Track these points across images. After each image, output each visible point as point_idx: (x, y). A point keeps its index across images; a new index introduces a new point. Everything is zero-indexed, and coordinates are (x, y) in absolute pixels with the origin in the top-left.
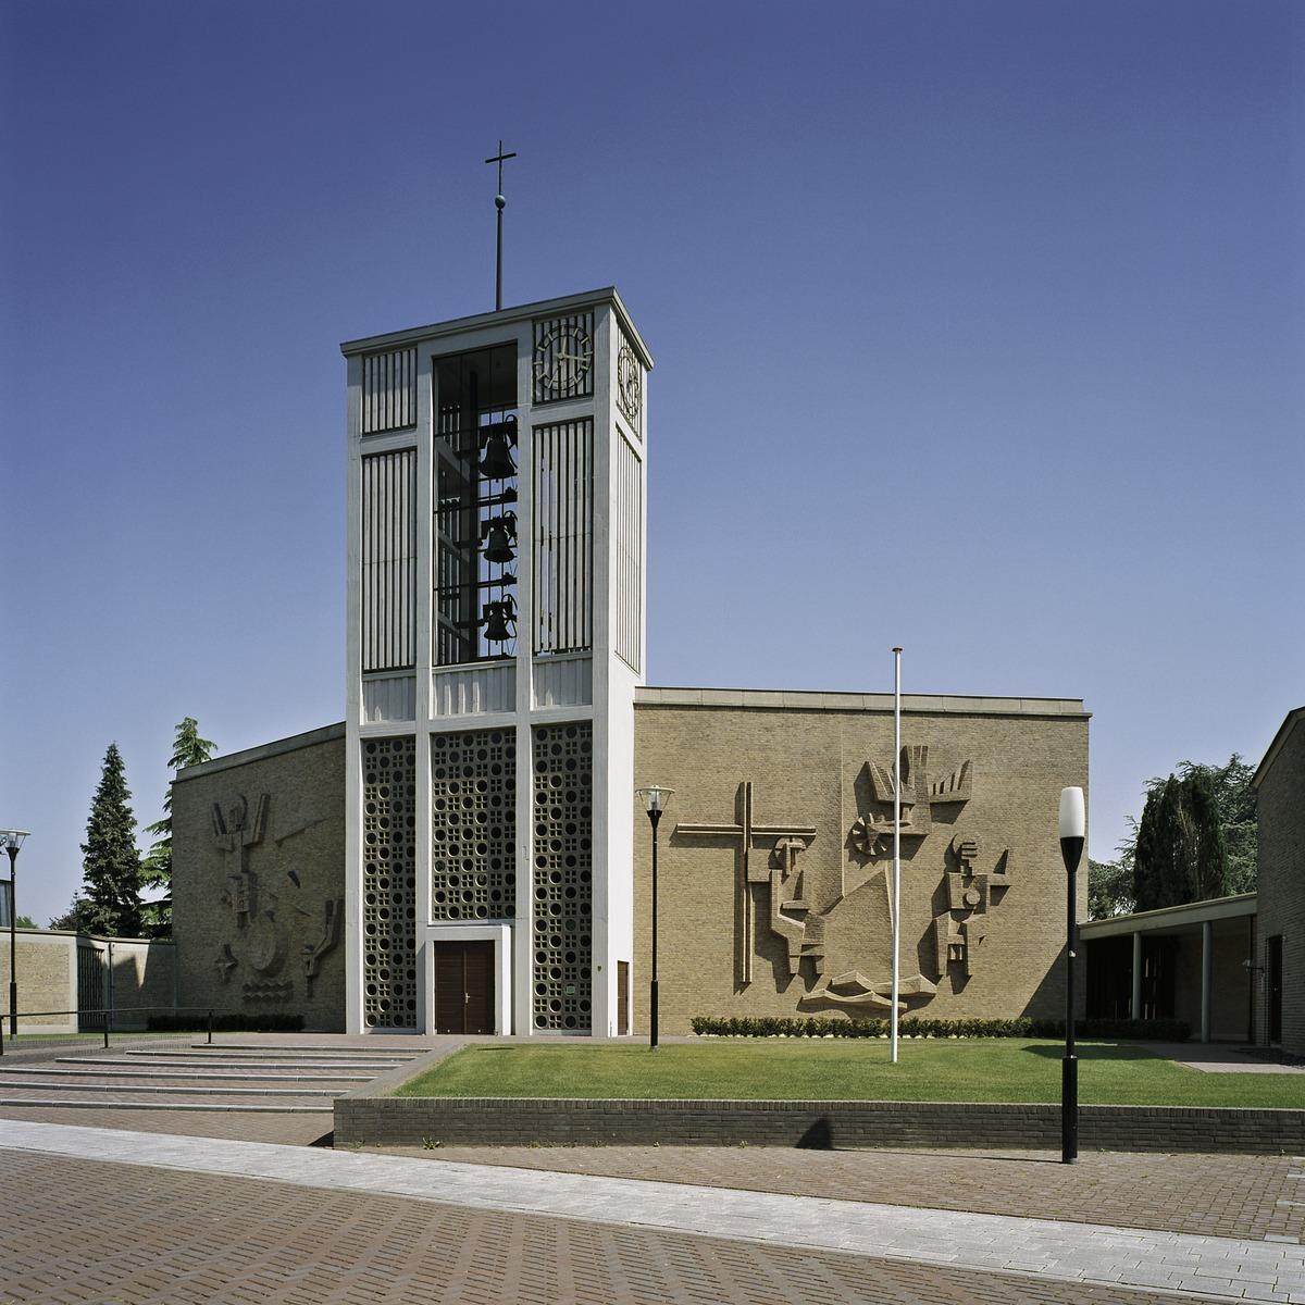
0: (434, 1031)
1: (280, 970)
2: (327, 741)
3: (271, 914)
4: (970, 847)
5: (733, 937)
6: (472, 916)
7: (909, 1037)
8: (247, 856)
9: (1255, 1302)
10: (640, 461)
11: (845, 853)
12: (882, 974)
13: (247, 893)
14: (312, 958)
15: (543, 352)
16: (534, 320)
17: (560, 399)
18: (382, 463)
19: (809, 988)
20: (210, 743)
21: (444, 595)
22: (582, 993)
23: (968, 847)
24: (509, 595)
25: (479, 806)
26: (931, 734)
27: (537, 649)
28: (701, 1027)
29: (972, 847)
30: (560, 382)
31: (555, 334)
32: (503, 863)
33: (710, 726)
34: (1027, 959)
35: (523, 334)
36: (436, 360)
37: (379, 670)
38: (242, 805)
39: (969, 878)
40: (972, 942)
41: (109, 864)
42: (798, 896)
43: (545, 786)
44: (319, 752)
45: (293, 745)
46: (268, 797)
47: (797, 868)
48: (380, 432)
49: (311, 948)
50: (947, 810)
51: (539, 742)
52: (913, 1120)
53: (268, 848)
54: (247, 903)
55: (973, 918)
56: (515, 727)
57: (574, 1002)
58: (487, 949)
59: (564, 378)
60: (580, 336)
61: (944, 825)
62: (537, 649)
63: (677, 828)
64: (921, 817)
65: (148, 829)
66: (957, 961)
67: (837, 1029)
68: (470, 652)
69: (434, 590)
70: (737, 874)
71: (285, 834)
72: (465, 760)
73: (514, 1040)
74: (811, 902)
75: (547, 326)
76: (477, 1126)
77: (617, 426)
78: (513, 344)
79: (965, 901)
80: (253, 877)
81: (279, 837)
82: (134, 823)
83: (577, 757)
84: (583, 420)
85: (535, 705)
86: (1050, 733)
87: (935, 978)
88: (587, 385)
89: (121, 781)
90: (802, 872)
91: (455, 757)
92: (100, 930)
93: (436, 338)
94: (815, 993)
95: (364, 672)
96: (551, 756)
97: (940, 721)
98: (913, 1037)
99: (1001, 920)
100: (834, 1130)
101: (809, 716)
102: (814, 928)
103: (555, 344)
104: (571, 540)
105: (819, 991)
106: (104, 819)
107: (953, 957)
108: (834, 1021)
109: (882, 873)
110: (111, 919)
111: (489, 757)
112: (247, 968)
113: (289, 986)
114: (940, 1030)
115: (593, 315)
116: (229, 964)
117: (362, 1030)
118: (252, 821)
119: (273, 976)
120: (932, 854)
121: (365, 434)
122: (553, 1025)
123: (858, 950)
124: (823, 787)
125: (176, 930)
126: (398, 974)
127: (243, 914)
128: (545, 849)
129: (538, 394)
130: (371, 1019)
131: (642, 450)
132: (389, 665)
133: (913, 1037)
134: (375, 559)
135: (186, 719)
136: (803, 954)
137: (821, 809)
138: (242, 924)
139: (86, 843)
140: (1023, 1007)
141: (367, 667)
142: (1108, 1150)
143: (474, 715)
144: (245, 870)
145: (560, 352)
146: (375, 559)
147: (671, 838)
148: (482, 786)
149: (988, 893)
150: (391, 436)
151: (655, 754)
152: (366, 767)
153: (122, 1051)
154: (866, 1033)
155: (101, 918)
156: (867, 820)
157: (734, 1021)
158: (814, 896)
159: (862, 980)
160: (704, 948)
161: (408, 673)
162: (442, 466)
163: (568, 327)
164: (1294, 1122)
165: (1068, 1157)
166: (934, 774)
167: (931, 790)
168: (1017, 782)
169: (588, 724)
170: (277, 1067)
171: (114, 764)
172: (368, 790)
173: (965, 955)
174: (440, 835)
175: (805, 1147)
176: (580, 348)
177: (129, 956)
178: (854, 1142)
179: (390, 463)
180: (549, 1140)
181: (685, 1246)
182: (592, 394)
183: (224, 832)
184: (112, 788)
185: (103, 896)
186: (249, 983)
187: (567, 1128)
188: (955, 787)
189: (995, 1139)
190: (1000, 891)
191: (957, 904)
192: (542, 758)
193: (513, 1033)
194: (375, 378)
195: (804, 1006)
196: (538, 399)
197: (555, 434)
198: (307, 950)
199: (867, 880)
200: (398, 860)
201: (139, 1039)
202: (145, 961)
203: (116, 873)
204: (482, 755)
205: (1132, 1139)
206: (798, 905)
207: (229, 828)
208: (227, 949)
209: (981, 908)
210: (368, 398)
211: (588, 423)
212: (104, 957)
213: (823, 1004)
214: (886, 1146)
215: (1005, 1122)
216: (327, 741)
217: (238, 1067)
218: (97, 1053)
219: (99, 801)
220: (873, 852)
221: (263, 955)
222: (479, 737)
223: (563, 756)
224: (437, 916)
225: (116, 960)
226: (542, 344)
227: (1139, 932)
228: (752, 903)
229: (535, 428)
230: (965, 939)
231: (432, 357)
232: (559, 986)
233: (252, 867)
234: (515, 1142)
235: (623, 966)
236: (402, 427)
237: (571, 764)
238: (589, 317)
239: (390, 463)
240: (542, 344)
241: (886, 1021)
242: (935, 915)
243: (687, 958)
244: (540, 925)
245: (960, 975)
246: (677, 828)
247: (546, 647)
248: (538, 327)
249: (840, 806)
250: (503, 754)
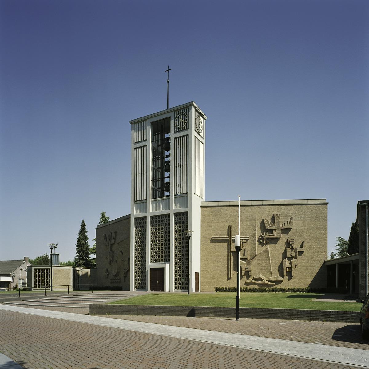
0: (150, 290)
2: (125, 219)
3: (116, 261)
4: (293, 241)
5: (227, 266)
7: (274, 292)
9: (364, 367)
10: (203, 144)
11: (257, 243)
12: (268, 275)
13: (111, 256)
14: (125, 272)
16: (174, 111)
17: (180, 131)
18: (139, 149)
19: (248, 279)
20: (108, 218)
21: (154, 181)
23: (292, 240)
25: (161, 234)
26: (281, 210)
27: (175, 194)
28: (217, 289)
29: (293, 240)
30: (181, 126)
31: (180, 114)
32: (167, 248)
33: (221, 211)
34: (309, 271)
35: (172, 115)
36: (152, 123)
37: (138, 201)
38: (111, 234)
39: (292, 249)
40: (293, 267)
41: (82, 249)
42: (244, 255)
43: (177, 228)
44: (127, 221)
45: (122, 219)
46: (116, 232)
47: (244, 247)
48: (139, 142)
49: (125, 269)
50: (286, 231)
51: (176, 217)
52: (211, 311)
54: (111, 258)
55: (294, 260)
56: (170, 214)
57: (184, 283)
58: (162, 270)
59: (182, 125)
61: (285, 235)
62: (175, 194)
63: (212, 238)
64: (278, 233)
65: (94, 240)
66: (289, 272)
67: (254, 290)
68: (162, 195)
69: (151, 180)
70: (228, 249)
72: (158, 222)
73: (169, 293)
74: (248, 256)
75: (178, 112)
76: (118, 311)
77: (195, 136)
78: (170, 117)
79: (291, 255)
81: (118, 242)
82: (88, 239)
83: (144, 225)
84: (186, 135)
85: (175, 208)
86: (316, 208)
87: (283, 276)
88: (187, 127)
89: (85, 228)
90: (245, 249)
91: (156, 222)
92: (79, 266)
94: (249, 281)
95: (135, 201)
96: (178, 220)
97: (284, 207)
98: (275, 292)
99: (302, 260)
100: (196, 313)
101: (247, 207)
102: (249, 263)
103: (179, 117)
104: (183, 166)
105: (250, 280)
106: (81, 238)
107: (288, 270)
108: (253, 288)
109: (267, 248)
110: (82, 263)
111: (164, 221)
112: (112, 275)
113: (120, 279)
114: (283, 290)
116: (107, 274)
117: (134, 290)
119: (117, 276)
120: (281, 244)
121: (135, 143)
122: (179, 289)
123: (261, 269)
124: (251, 226)
125: (97, 265)
127: (111, 261)
128: (177, 244)
129: (176, 130)
130: (136, 287)
131: (204, 141)
132: (141, 199)
133: (275, 292)
134: (137, 174)
135: (103, 212)
136: (246, 270)
137: (251, 232)
138: (110, 264)
139: (77, 244)
140: (309, 284)
141: (136, 200)
142: (254, 318)
143: (161, 211)
144: (111, 250)
145: (181, 118)
146: (137, 174)
147: (210, 241)
148: (162, 229)
149: (298, 253)
150: (180, 132)
151: (206, 219)
152: (135, 225)
153: (72, 295)
154: (262, 291)
155: (80, 263)
156: (263, 234)
157: (226, 288)
158: (249, 255)
159: (262, 277)
160: (219, 269)
161: (186, 195)
162: (153, 149)
163: (182, 112)
164: (296, 312)
165: (237, 319)
166: (282, 222)
167: (281, 226)
168: (307, 222)
169: (187, 213)
170: (101, 299)
171: (83, 224)
172: (176, 227)
173: (291, 270)
174: (152, 241)
175: (188, 317)
176: (185, 117)
177: (87, 272)
178: (199, 316)
179: (141, 149)
180: (133, 314)
181: (228, 350)
182: (188, 129)
183: (107, 241)
184: (83, 231)
185: (81, 257)
186: (112, 278)
187: (137, 311)
188: (288, 224)
189: (229, 315)
190: (301, 253)
191: (289, 256)
192: (176, 221)
193: (169, 291)
194: (138, 129)
195: (246, 284)
197: (179, 139)
198: (124, 270)
199: (263, 250)
200: (183, 245)
201: (80, 292)
202: (90, 272)
203: (84, 251)
204: (162, 221)
205: (260, 316)
206: (244, 257)
207: (108, 240)
208: (107, 270)
209: (296, 257)
210: (136, 133)
211: (187, 136)
212: (80, 273)
213: (251, 283)
214: (205, 316)
215: (232, 311)
216: (125, 219)
217: (93, 298)
218: (67, 295)
219: (80, 234)
220: (265, 243)
221: (115, 271)
222: (179, 214)
223: (181, 221)
224: (152, 262)
225: (84, 273)
226: (176, 117)
227: (338, 263)
228: (232, 257)
229: (175, 138)
230: (291, 266)
231: (151, 122)
232: (180, 279)
233: (113, 250)
234: (126, 314)
235: (197, 274)
236: (144, 140)
237: (183, 223)
238: (187, 109)
239: (141, 149)
240: (176, 117)
241: (268, 288)
242: (283, 260)
243: (215, 271)
244: (176, 263)
245: (290, 276)
246: (212, 238)
248: (176, 113)
249: (256, 231)
250: (167, 220)
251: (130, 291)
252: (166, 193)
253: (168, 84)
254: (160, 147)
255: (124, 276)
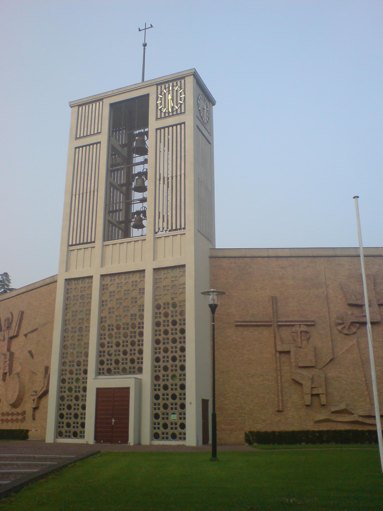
1: (20, 405)
6: (103, 373)
8: (11, 343)
14: (36, 398)
15: (161, 98)
22: (180, 418)
24: (145, 207)
38: (11, 317)
45: (37, 286)
49: (36, 392)
53: (21, 338)
60: (179, 89)
71: (29, 331)
80: (12, 354)
93: (112, 96)
113: (24, 413)
115: (185, 81)
118: (14, 324)
126: (166, 397)
127: (5, 373)
144: (9, 350)
163: (173, 86)
182: (184, 112)
196: (159, 117)
198: (34, 393)
211: (183, 125)
233: (13, 349)
238: (183, 81)
247: (161, 229)
251: (98, 389)
252: (135, 232)
253: (144, 49)
254: (126, 149)
255: (34, 406)
